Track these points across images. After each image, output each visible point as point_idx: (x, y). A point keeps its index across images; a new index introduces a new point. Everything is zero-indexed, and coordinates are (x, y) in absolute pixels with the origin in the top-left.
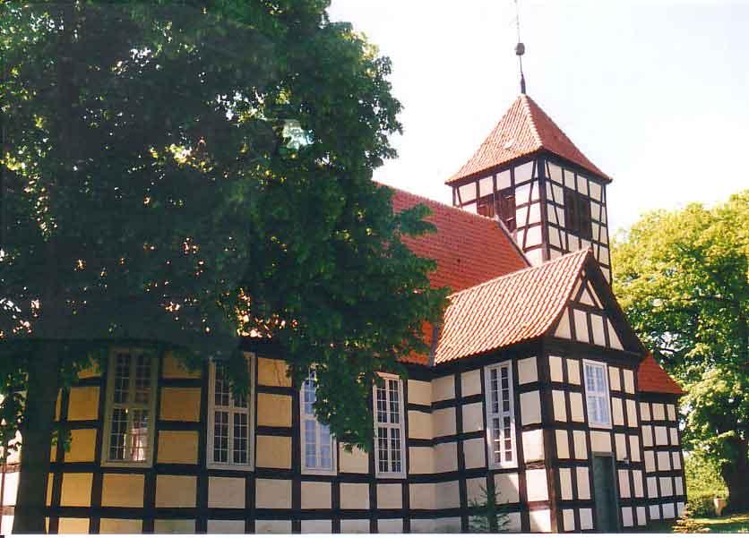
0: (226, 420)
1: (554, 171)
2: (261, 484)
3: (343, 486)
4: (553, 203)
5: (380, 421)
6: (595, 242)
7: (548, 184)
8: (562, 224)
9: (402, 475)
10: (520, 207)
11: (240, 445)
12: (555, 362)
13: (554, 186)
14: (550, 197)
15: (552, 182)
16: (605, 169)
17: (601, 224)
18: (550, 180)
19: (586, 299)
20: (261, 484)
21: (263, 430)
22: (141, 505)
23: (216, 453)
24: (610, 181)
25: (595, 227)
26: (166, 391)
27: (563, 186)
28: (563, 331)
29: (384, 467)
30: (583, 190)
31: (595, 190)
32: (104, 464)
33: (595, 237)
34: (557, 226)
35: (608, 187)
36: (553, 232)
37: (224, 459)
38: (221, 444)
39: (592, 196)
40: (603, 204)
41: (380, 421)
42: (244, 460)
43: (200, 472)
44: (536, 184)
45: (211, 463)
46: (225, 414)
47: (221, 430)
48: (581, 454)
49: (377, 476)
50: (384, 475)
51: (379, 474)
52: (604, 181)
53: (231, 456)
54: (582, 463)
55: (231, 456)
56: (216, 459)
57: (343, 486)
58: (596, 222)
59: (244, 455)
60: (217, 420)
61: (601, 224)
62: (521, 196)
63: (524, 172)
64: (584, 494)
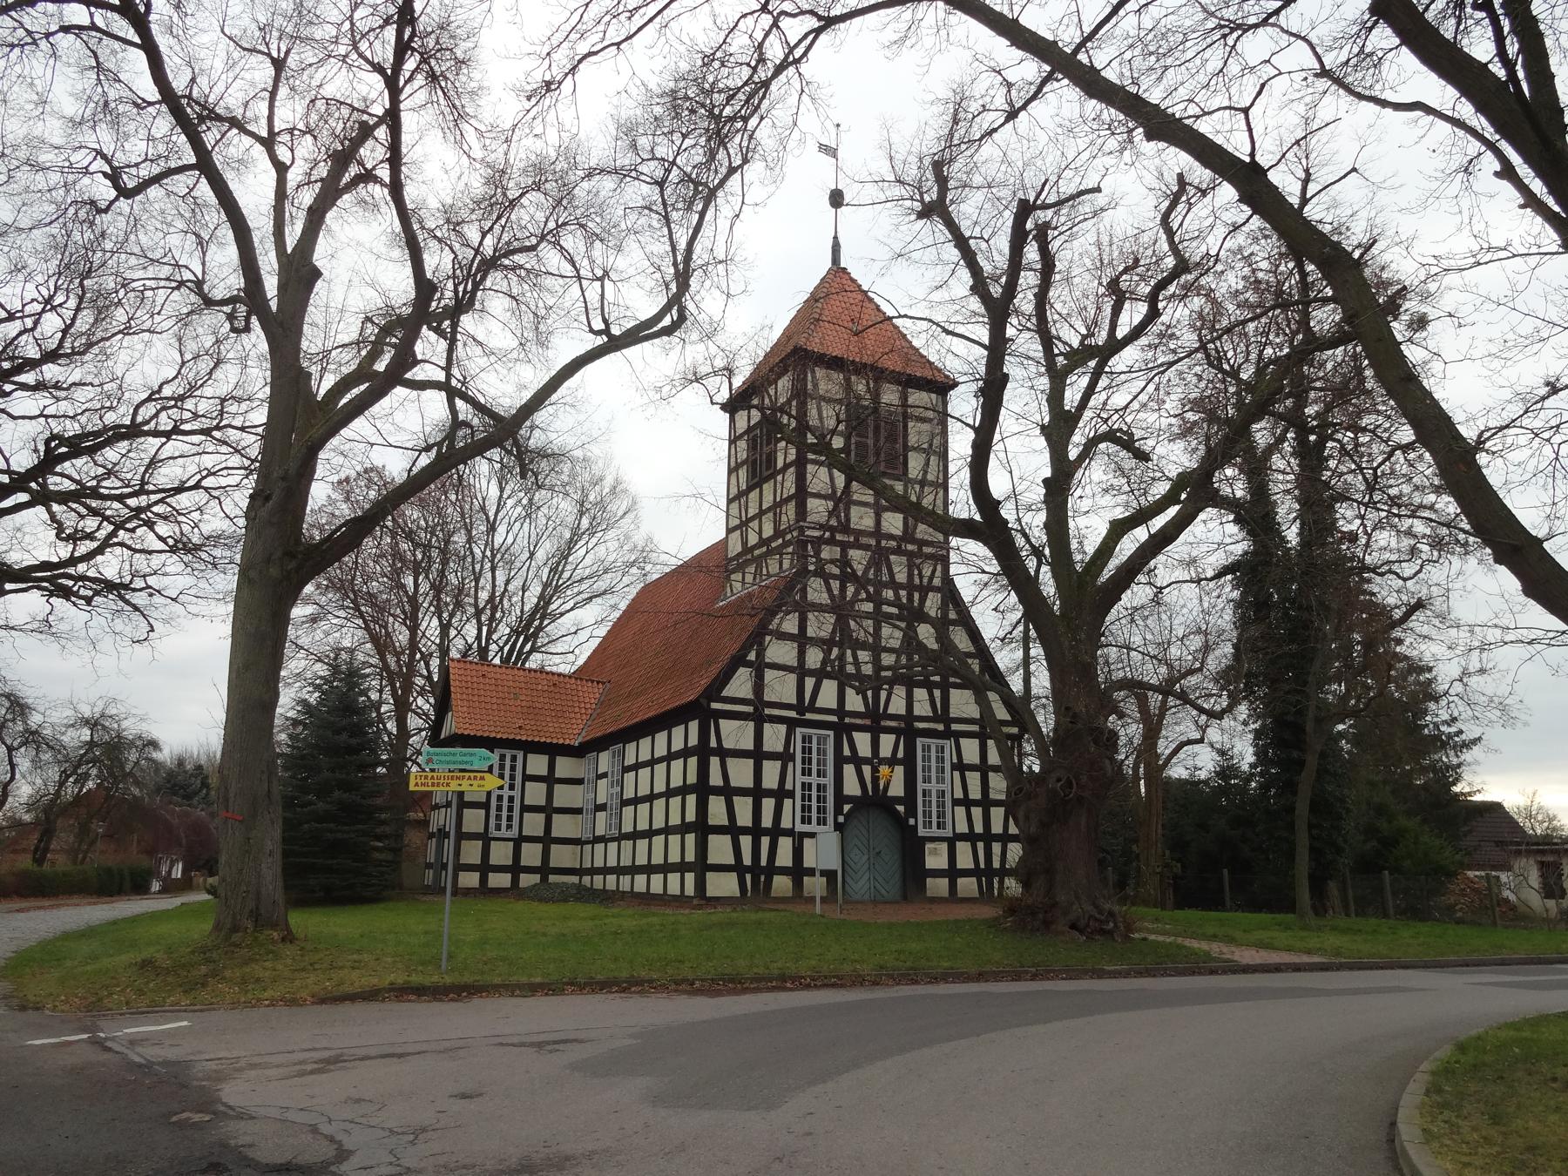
29: (498, 828)
37: (810, 823)
46: (810, 784)
51: (494, 833)
60: (803, 789)
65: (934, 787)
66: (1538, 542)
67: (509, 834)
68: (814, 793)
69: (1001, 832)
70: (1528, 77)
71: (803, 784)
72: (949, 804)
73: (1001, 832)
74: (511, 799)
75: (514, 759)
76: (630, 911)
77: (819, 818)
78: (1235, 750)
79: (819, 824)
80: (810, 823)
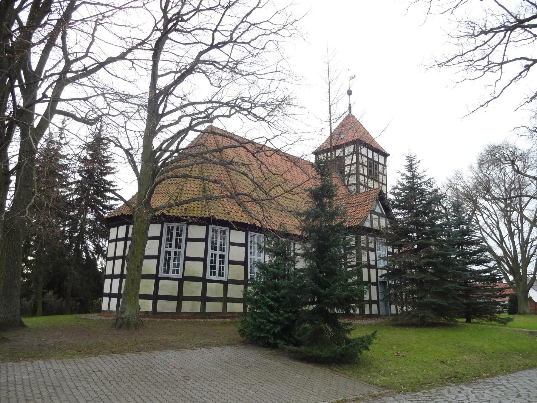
0: (215, 257)
1: (364, 151)
2: (230, 286)
3: (185, 283)
4: (362, 164)
5: (212, 249)
6: (380, 183)
7: (360, 155)
8: (366, 174)
9: (180, 276)
10: (347, 165)
11: (221, 268)
12: (363, 238)
13: (363, 157)
14: (361, 161)
15: (362, 155)
16: (387, 150)
17: (383, 175)
18: (361, 154)
19: (378, 210)
20: (230, 286)
21: (231, 262)
22: (208, 295)
23: (211, 272)
24: (388, 155)
25: (381, 176)
26: (189, 243)
27: (367, 157)
28: (367, 224)
29: (213, 273)
30: (376, 159)
31: (382, 160)
32: (159, 276)
33: (381, 181)
34: (363, 175)
35: (387, 158)
36: (361, 178)
37: (214, 275)
38: (213, 267)
39: (380, 162)
40: (385, 166)
41: (212, 249)
42: (223, 276)
43: (204, 280)
44: (355, 156)
45: (209, 277)
46: (215, 255)
47: (213, 262)
48: (373, 279)
49: (207, 278)
50: (165, 275)
51: (161, 274)
52: (386, 155)
53: (217, 273)
54: (374, 284)
55: (217, 273)
56: (211, 275)
57: (185, 283)
58: (381, 174)
59: (223, 273)
60: (212, 257)
61: (383, 175)
62: (348, 161)
63: (350, 149)
64: (374, 298)
65: (218, 253)
66: (158, 70)
67: (175, 276)
68: (218, 259)
69: (117, 292)
70: (6, 189)
71: (212, 254)
72: (226, 262)
73: (117, 292)
76: (267, 352)
77: (220, 273)
78: (81, 144)
79: (219, 276)
80: (214, 275)
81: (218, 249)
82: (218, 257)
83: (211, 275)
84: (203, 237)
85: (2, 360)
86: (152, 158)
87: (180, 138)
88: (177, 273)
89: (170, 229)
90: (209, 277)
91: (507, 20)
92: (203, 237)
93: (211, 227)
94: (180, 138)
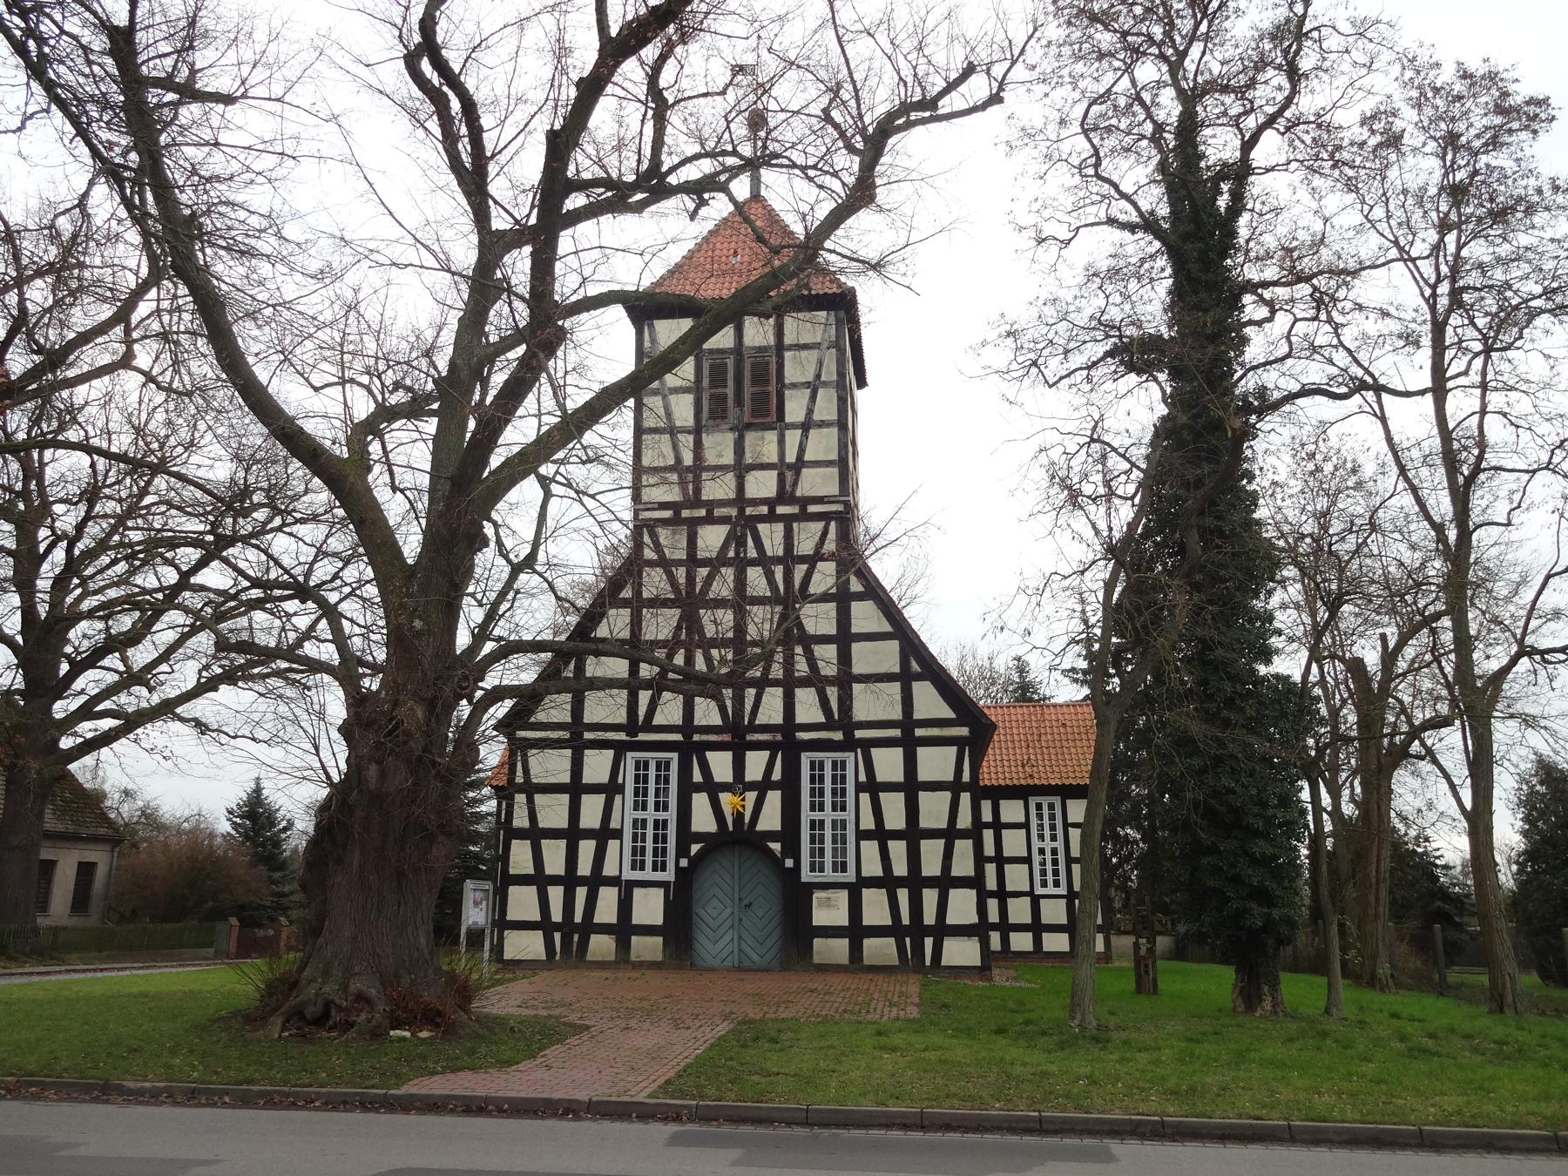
29: (1044, 884)
37: (642, 868)
42: (664, 869)
57: (1027, 900)
67: (840, 877)
74: (1054, 852)
75: (1051, 807)
81: (828, 825)
82: (650, 825)
83: (633, 868)
84: (1022, 819)
85: (9, 1091)
86: (1373, 751)
87: (1470, 748)
88: (844, 869)
89: (642, 765)
90: (1039, 891)
91: (277, 184)
92: (1022, 819)
93: (1033, 801)
94: (1470, 748)
